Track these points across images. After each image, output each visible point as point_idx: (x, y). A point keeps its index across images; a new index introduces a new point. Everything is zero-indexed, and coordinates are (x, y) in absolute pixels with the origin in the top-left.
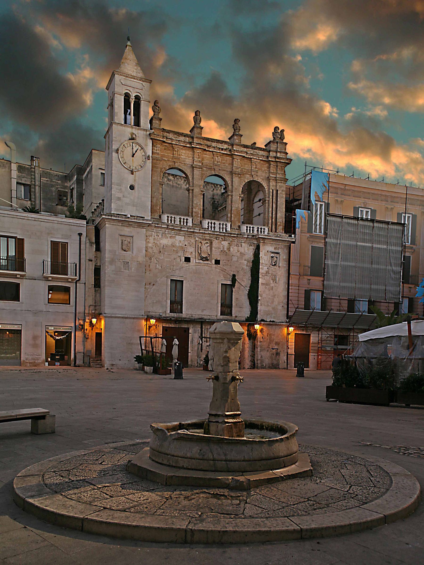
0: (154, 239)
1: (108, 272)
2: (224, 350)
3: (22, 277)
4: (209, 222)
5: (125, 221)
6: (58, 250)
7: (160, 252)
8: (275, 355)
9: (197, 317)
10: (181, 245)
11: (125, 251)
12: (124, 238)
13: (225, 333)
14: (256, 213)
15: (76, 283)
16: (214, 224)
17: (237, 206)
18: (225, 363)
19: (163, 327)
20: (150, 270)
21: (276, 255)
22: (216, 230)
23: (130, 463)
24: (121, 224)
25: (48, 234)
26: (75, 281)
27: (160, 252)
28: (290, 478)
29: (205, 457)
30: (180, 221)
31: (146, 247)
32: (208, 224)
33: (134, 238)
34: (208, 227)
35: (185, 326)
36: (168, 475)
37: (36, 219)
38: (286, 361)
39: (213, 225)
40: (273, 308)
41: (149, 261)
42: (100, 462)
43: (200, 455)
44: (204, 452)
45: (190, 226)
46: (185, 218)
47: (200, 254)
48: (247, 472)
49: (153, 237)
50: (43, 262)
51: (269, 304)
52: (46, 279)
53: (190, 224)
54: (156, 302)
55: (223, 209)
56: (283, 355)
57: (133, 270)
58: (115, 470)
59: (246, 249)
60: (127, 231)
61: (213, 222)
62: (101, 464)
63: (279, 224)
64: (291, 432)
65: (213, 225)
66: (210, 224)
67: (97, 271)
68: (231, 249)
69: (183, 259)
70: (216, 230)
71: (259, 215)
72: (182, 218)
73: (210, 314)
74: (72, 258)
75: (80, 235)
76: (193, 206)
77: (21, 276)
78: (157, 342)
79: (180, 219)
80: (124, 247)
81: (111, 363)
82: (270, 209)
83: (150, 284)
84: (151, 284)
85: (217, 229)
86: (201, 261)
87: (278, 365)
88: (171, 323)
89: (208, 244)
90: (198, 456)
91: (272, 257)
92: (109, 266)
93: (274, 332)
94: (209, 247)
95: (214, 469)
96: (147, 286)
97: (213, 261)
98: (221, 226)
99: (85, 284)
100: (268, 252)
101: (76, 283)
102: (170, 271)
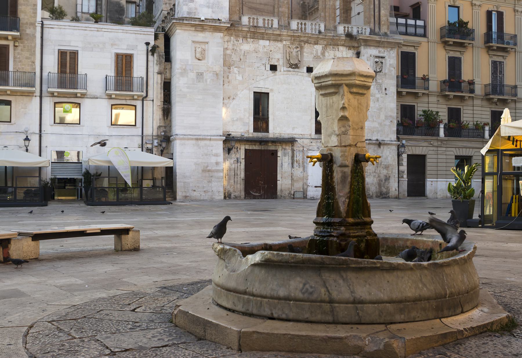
0: (234, 45)
1: (179, 85)
2: (341, 106)
3: (83, 96)
4: (298, 23)
5: (201, 25)
6: (124, 63)
7: (241, 59)
8: (384, 181)
9: (286, 136)
10: (265, 50)
11: (199, 60)
12: (198, 45)
13: (342, 75)
14: (354, 13)
15: (143, 100)
16: (305, 24)
17: (331, 4)
18: (343, 129)
19: (246, 150)
20: (229, 82)
21: (381, 59)
22: (307, 31)
23: (178, 310)
24: (194, 29)
25: (112, 45)
26: (141, 98)
27: (241, 59)
28: (475, 335)
29: (315, 296)
30: (264, 23)
31: (225, 55)
32: (298, 25)
33: (210, 44)
34: (298, 28)
35: (272, 147)
36: (243, 330)
37: (99, 30)
38: (397, 189)
39: (303, 26)
40: (380, 124)
41: (228, 70)
42: (132, 308)
43: (303, 293)
44: (311, 287)
45: (275, 28)
46: (270, 19)
47: (289, 61)
48: (395, 323)
49: (232, 42)
50: (106, 78)
51: (375, 120)
52: (110, 97)
53: (276, 25)
54: (237, 120)
55: (314, 10)
56: (393, 181)
57: (208, 82)
58: (153, 321)
59: (344, 53)
60: (201, 36)
61: (303, 23)
62: (133, 310)
63: (383, 23)
64: (470, 250)
65: (303, 26)
66: (300, 25)
67: (167, 87)
68: (326, 54)
69: (268, 67)
70: (307, 31)
71: (359, 14)
72: (266, 19)
73: (302, 133)
74: (138, 70)
75: (148, 44)
76: (279, 4)
77: (81, 95)
78: (239, 168)
79: (264, 20)
80: (198, 55)
81: (184, 194)
82: (372, 6)
83: (229, 98)
84: (231, 98)
85: (308, 31)
86: (290, 69)
87: (388, 193)
88: (255, 145)
89: (298, 49)
90: (300, 296)
91: (376, 62)
92: (181, 78)
93: (382, 153)
94: (299, 52)
95: (330, 318)
96: (225, 101)
97: (305, 69)
98: (314, 27)
99: (153, 101)
100: (371, 56)
101: (143, 100)
102: (253, 82)
